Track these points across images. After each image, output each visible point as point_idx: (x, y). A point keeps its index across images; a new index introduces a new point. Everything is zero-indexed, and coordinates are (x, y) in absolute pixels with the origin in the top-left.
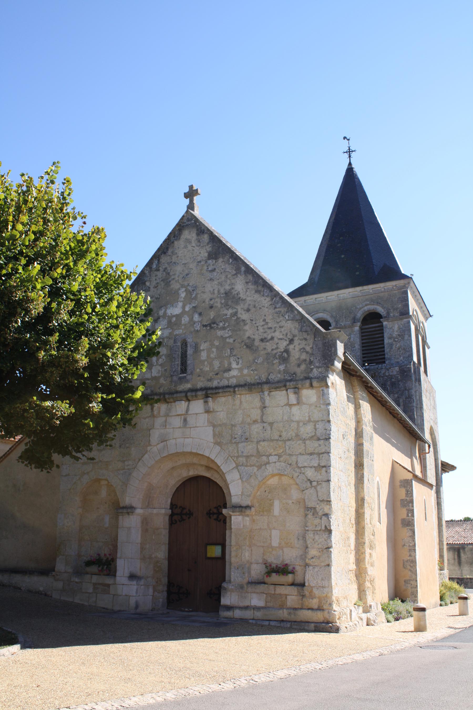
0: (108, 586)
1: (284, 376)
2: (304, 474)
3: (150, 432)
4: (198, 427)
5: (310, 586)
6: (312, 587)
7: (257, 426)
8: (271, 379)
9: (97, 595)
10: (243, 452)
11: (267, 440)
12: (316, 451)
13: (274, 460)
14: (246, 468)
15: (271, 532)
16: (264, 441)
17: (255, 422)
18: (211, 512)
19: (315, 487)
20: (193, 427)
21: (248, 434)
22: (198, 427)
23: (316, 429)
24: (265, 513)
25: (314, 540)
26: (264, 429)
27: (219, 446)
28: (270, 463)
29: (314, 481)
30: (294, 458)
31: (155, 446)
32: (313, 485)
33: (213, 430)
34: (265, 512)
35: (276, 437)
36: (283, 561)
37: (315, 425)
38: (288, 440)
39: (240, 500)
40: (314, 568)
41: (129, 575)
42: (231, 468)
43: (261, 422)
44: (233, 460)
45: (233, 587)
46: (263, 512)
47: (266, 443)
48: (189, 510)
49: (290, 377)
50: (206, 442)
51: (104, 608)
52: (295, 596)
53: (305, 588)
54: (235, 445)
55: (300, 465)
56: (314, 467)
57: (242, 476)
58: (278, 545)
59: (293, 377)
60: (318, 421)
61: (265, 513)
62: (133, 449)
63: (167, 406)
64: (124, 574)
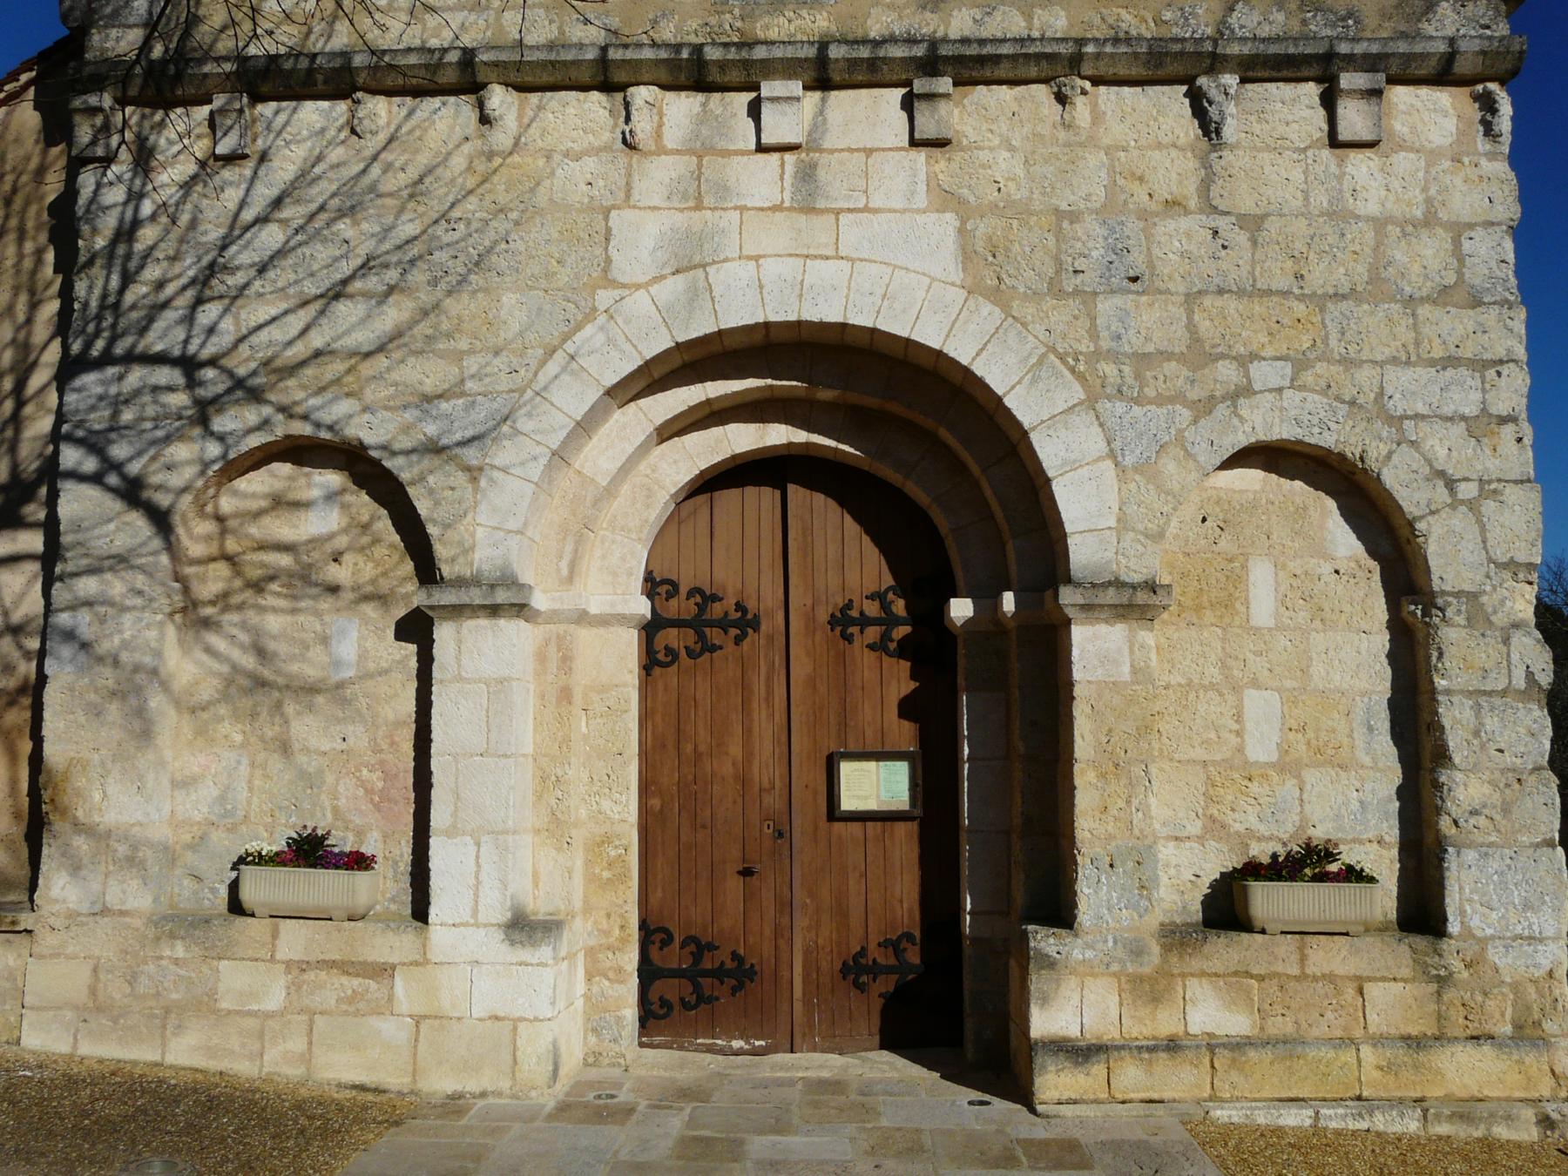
0: (383, 971)
1: (1304, 22)
2: (1418, 449)
3: (606, 219)
4: (876, 211)
5: (1474, 936)
6: (1483, 942)
7: (1185, 223)
8: (1242, 27)
9: (311, 1023)
10: (1119, 337)
11: (1235, 289)
12: (1467, 352)
13: (1275, 382)
14: (1135, 408)
15: (1241, 700)
16: (1221, 291)
17: (1173, 205)
18: (854, 613)
19: (1472, 505)
20: (850, 210)
21: (1142, 258)
22: (876, 211)
23: (1461, 259)
24: (1209, 616)
25: (1477, 734)
26: (1220, 242)
27: (995, 303)
28: (1256, 393)
29: (1466, 479)
30: (1366, 377)
31: (638, 287)
32: (1460, 496)
33: (961, 231)
34: (1208, 612)
35: (1281, 282)
36: (1304, 823)
37: (1457, 243)
38: (1336, 295)
39: (1110, 554)
40: (1486, 854)
41: (509, 915)
42: (1062, 406)
43: (1201, 211)
44: (1072, 370)
45: (1089, 954)
46: (1198, 609)
47: (1232, 305)
48: (740, 607)
49: (1334, 26)
50: (927, 281)
51: (362, 1088)
52: (1405, 980)
53: (1445, 945)
54: (1074, 305)
55: (1398, 405)
56: (1463, 418)
57: (1117, 445)
58: (1274, 757)
59: (1348, 27)
60: (1471, 226)
61: (1209, 616)
62: (509, 299)
63: (704, 105)
64: (475, 912)
